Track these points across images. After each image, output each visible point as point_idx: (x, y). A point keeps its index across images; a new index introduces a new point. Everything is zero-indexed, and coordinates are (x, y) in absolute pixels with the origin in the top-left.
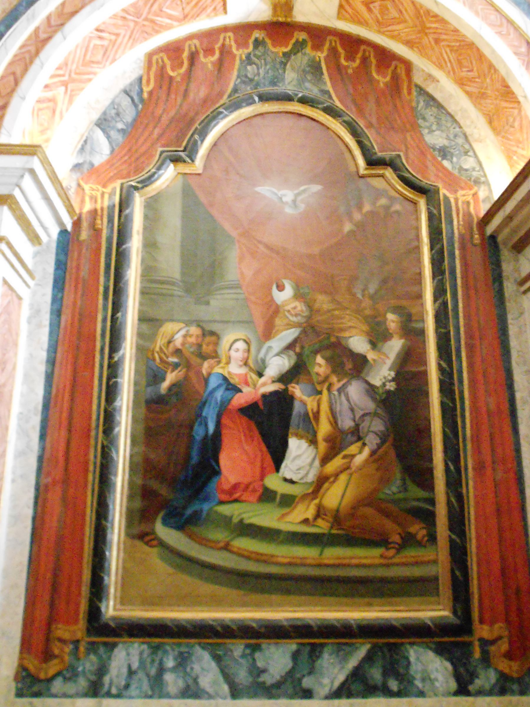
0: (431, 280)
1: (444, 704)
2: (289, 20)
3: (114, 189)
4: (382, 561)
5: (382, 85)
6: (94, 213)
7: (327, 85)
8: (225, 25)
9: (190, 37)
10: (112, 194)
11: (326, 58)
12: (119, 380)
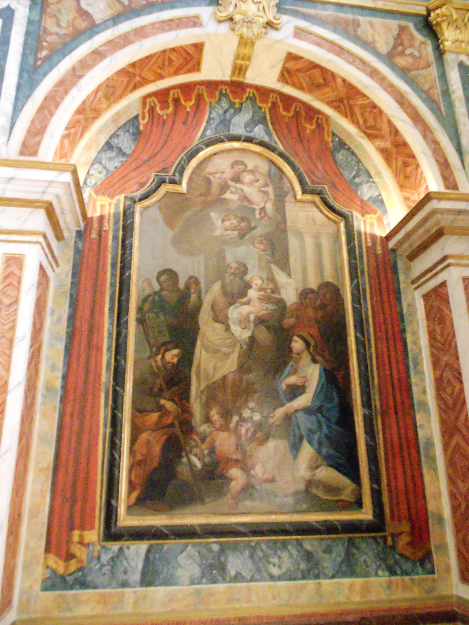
3: (119, 201)
5: (308, 131)
6: (101, 218)
9: (174, 87)
10: (117, 206)
12: (170, 233)
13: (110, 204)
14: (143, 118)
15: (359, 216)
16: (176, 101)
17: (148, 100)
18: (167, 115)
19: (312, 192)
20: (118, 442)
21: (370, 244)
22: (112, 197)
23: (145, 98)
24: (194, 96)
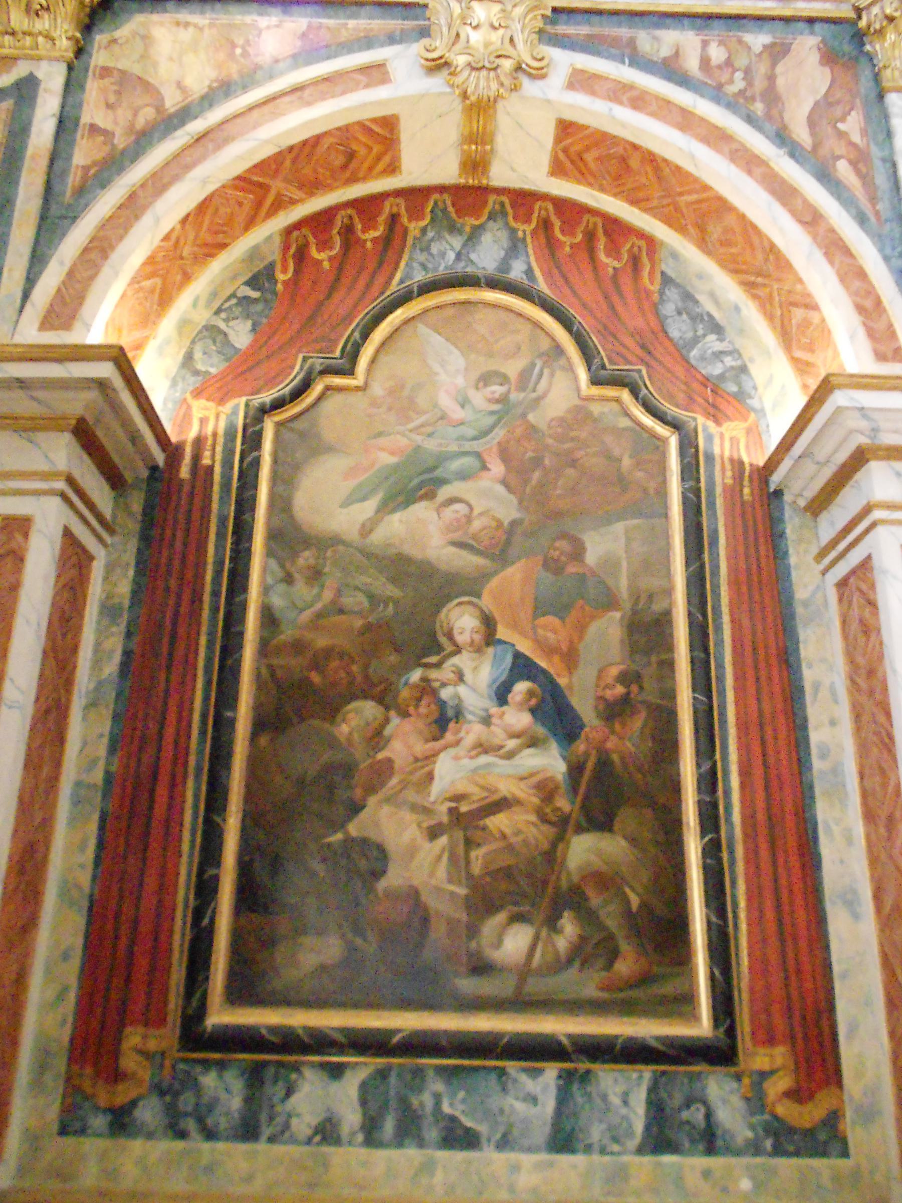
0: (684, 569)
1: (693, 1180)
2: (484, 182)
3: (237, 406)
4: (605, 995)
6: (199, 442)
7: (398, 1093)
8: (633, 82)
11: (534, 233)
13: (217, 417)
14: (285, 270)
15: (711, 424)
16: (348, 230)
17: (295, 234)
18: (330, 259)
19: (617, 382)
20: (714, 919)
21: (729, 481)
22: (222, 401)
23: (288, 231)
24: (382, 219)
